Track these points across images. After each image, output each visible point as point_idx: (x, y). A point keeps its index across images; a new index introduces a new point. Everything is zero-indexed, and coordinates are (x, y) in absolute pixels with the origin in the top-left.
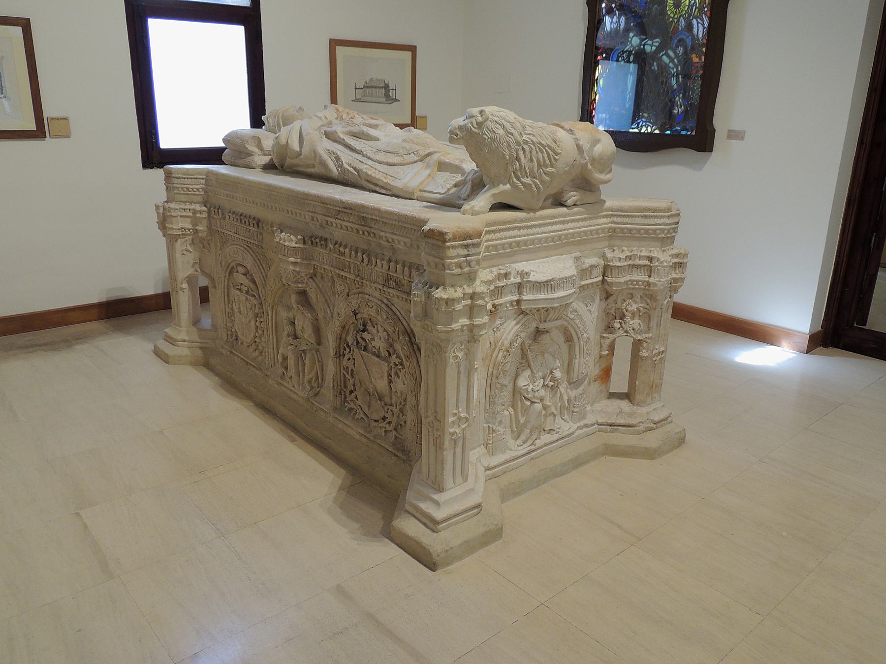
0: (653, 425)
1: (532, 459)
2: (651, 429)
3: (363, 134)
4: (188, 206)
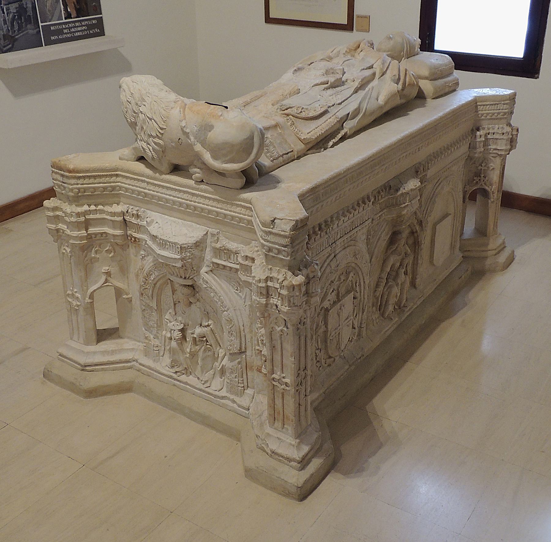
1: (174, 385)
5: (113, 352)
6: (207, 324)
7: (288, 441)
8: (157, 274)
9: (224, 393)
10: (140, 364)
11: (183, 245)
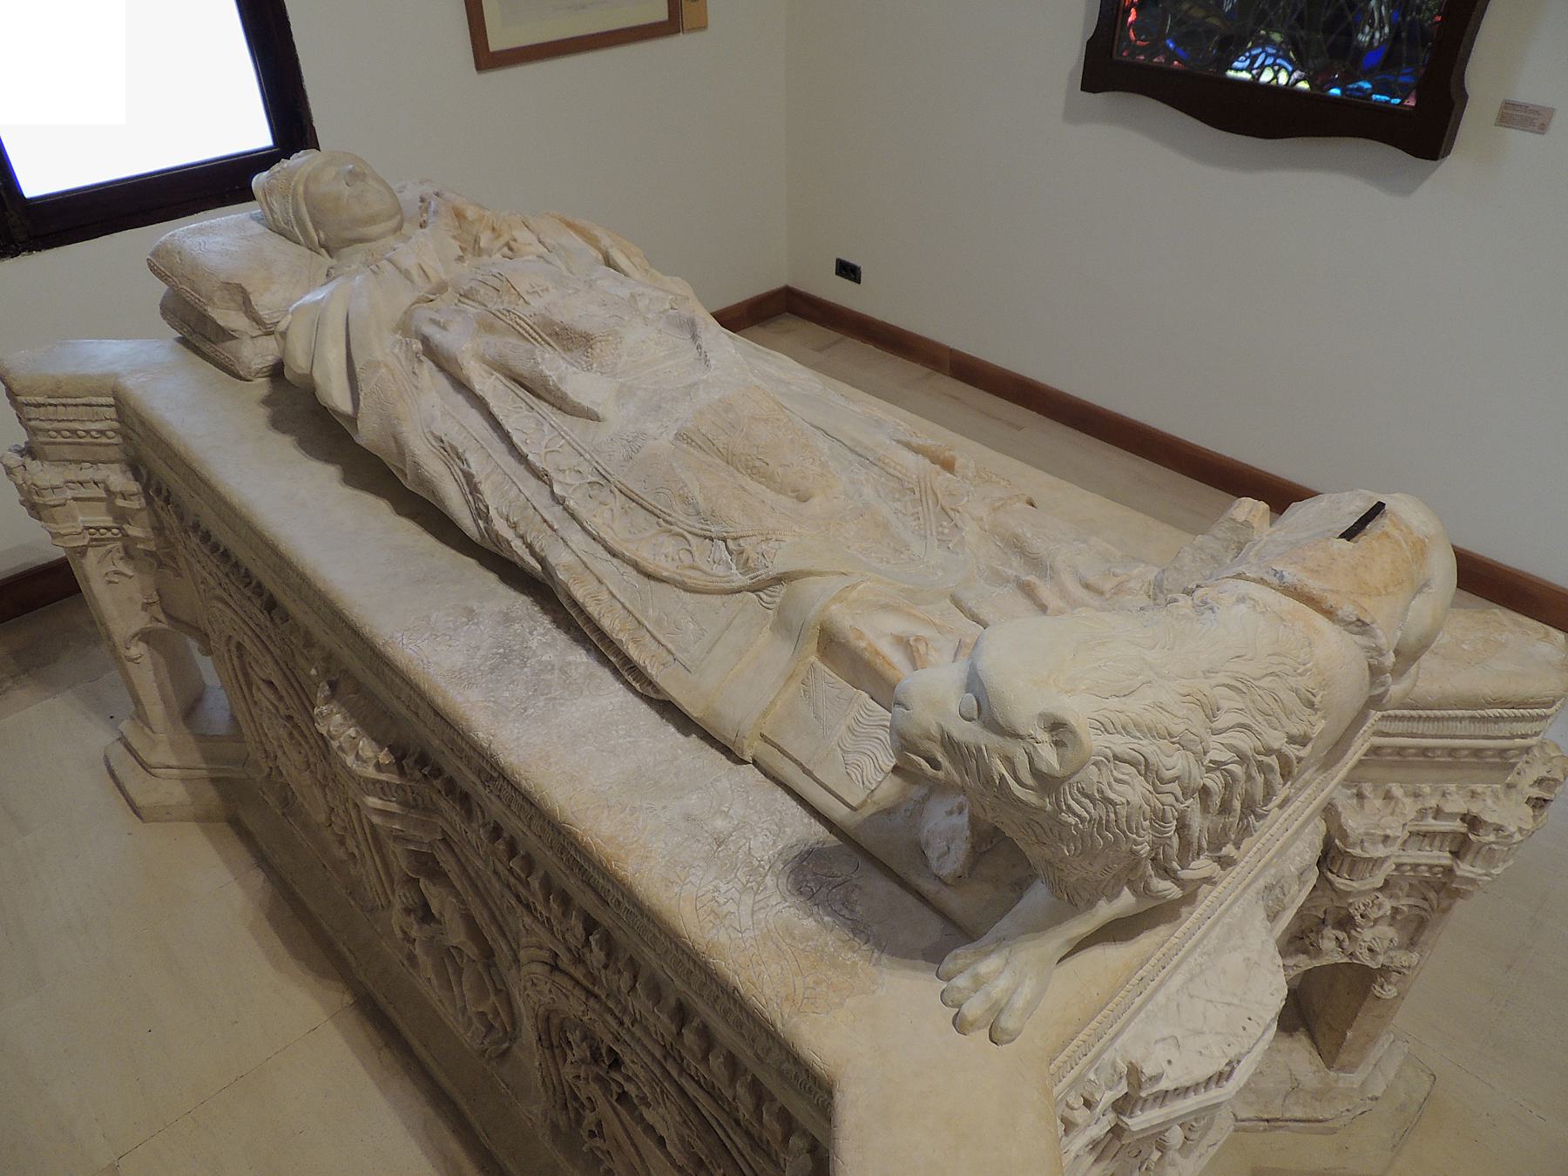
3: (545, 385)
4: (88, 473)
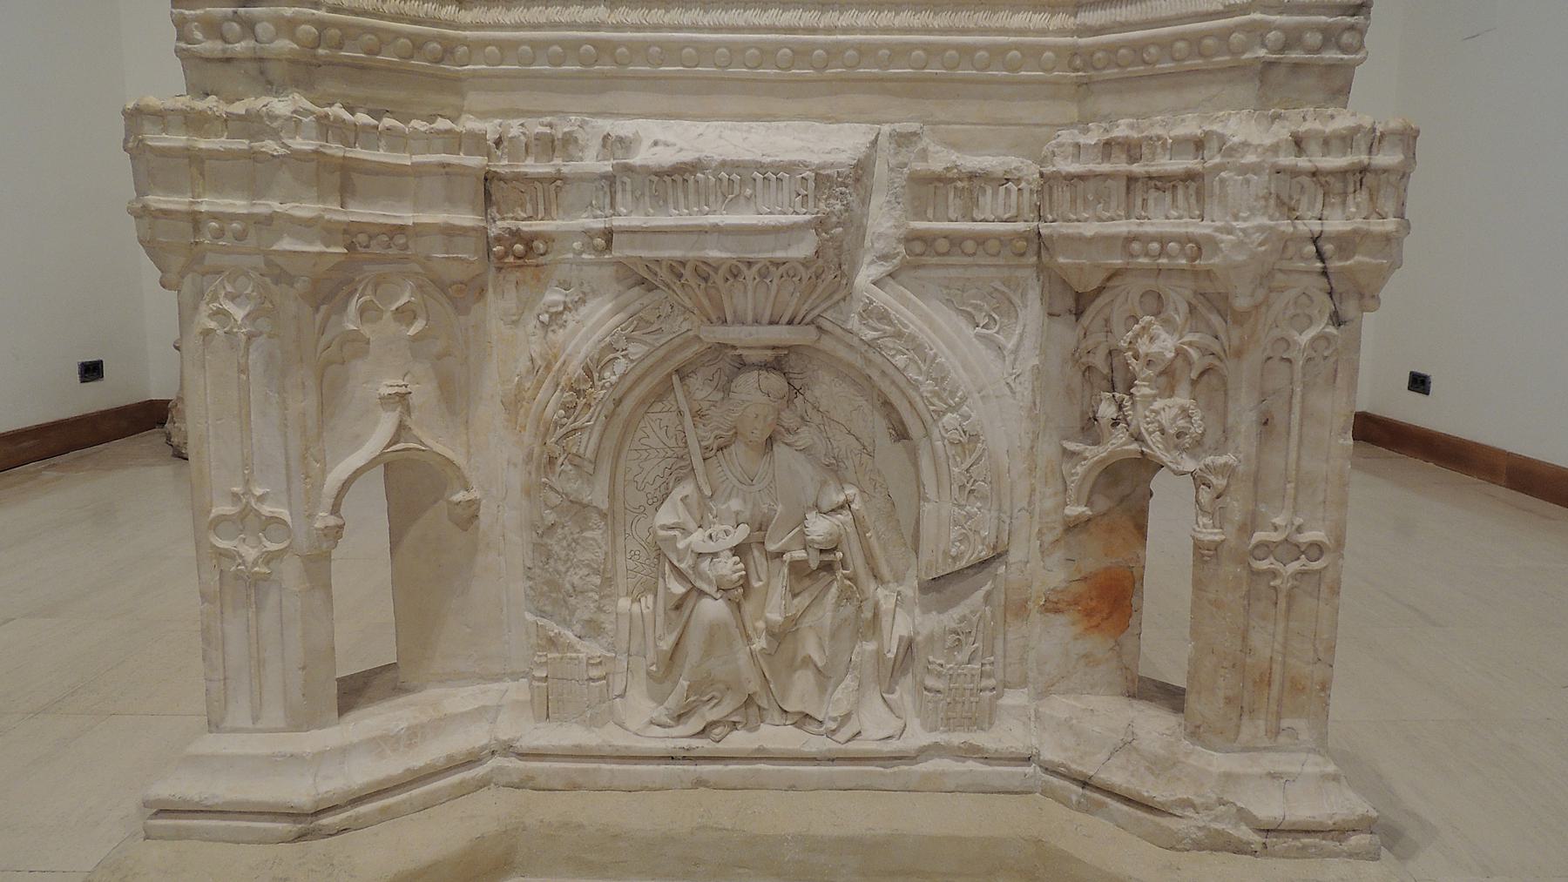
0: (1245, 833)
1: (699, 783)
2: (1240, 848)
5: (414, 735)
6: (842, 498)
7: (1309, 769)
8: (636, 350)
9: (918, 737)
10: (523, 756)
11: (823, 168)
